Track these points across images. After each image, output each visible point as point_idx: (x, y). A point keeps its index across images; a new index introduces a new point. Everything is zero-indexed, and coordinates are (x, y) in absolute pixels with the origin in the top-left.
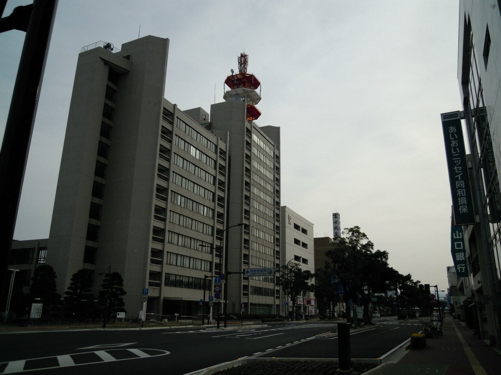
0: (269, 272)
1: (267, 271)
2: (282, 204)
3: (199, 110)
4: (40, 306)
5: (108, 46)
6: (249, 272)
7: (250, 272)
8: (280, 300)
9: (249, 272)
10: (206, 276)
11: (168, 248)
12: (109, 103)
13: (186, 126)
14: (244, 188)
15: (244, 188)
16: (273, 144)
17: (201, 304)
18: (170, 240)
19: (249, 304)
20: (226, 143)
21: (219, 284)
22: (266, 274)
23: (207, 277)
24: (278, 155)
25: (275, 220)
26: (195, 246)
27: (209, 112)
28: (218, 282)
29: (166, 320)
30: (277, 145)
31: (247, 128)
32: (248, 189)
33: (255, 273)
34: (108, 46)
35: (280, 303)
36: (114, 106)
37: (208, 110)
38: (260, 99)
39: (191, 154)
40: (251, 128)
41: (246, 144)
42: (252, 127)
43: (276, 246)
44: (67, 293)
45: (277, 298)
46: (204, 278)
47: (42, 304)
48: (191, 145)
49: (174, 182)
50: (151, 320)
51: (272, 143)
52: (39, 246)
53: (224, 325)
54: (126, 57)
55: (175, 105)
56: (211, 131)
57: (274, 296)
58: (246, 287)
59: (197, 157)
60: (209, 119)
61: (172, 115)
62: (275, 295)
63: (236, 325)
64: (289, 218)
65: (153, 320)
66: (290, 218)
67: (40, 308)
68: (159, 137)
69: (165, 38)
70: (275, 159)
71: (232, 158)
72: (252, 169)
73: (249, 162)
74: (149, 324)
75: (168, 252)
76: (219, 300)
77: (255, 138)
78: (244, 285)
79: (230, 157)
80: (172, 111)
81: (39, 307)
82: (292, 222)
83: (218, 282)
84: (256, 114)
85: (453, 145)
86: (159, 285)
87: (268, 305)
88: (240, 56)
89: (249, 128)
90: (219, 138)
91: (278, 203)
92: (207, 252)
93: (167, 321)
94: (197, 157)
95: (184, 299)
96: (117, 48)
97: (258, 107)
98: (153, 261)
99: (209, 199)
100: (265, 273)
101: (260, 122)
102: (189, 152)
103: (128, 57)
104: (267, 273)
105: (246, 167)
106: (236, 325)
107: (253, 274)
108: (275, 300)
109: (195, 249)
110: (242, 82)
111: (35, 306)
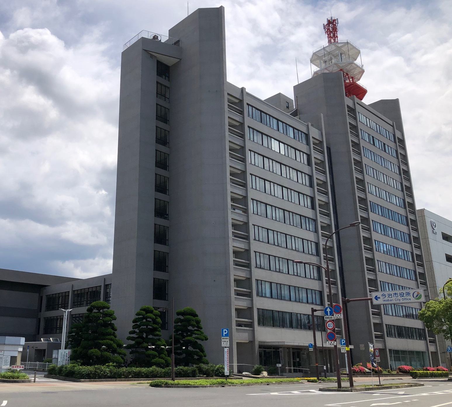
0: (415, 296)
1: (411, 295)
2: (418, 207)
3: (279, 96)
4: (68, 353)
5: (155, 37)
6: (379, 298)
7: (381, 297)
8: (436, 345)
9: (379, 298)
10: (313, 311)
11: (257, 274)
12: (162, 102)
13: (261, 113)
14: (356, 188)
15: (356, 188)
16: (392, 124)
17: (311, 349)
18: (258, 263)
19: (388, 350)
20: (320, 130)
21: (331, 318)
22: (410, 299)
23: (316, 311)
24: (400, 137)
25: (411, 228)
26: (295, 271)
27: (293, 99)
28: (329, 314)
29: (265, 374)
30: (398, 124)
31: (348, 106)
32: (359, 169)
33: (391, 299)
34: (155, 37)
35: (437, 348)
36: (166, 105)
37: (291, 95)
38: (363, 71)
39: (273, 149)
40: (354, 104)
41: (352, 145)
42: (356, 104)
43: (418, 265)
44: (129, 338)
45: (433, 342)
46: (311, 313)
47: (70, 350)
48: (271, 137)
49: (254, 187)
50: (244, 373)
51: (391, 123)
52: (104, 283)
53: (36, 380)
54: (175, 44)
55: (243, 89)
56: (298, 116)
57: (425, 339)
58: (378, 326)
59: (282, 152)
60: (294, 105)
61: (241, 101)
62: (428, 338)
63: (346, 388)
64: (433, 225)
65: (247, 373)
66: (434, 225)
67: (68, 355)
68: (227, 133)
69: (218, 6)
70: (398, 144)
71: (332, 150)
72: (360, 126)
73: (354, 117)
74: (242, 378)
75: (257, 280)
76: (335, 342)
77: (362, 118)
78: (374, 324)
79: (329, 149)
80: (238, 96)
81: (67, 354)
82: (439, 230)
83: (329, 314)
84: (361, 92)
85: (225, 332)
86: (251, 325)
87: (418, 353)
88: (326, 23)
89: (351, 105)
90: (310, 124)
91: (412, 205)
92: (312, 277)
93: (267, 375)
94: (282, 152)
95: (286, 344)
96: (164, 37)
97: (362, 82)
98: (238, 294)
99: (306, 206)
100: (409, 297)
101: (367, 100)
102: (270, 148)
103: (177, 43)
104: (411, 297)
105: (356, 178)
106: (346, 388)
107: (387, 301)
108: (429, 346)
109: (296, 274)
110: (333, 55)
111: (62, 353)
